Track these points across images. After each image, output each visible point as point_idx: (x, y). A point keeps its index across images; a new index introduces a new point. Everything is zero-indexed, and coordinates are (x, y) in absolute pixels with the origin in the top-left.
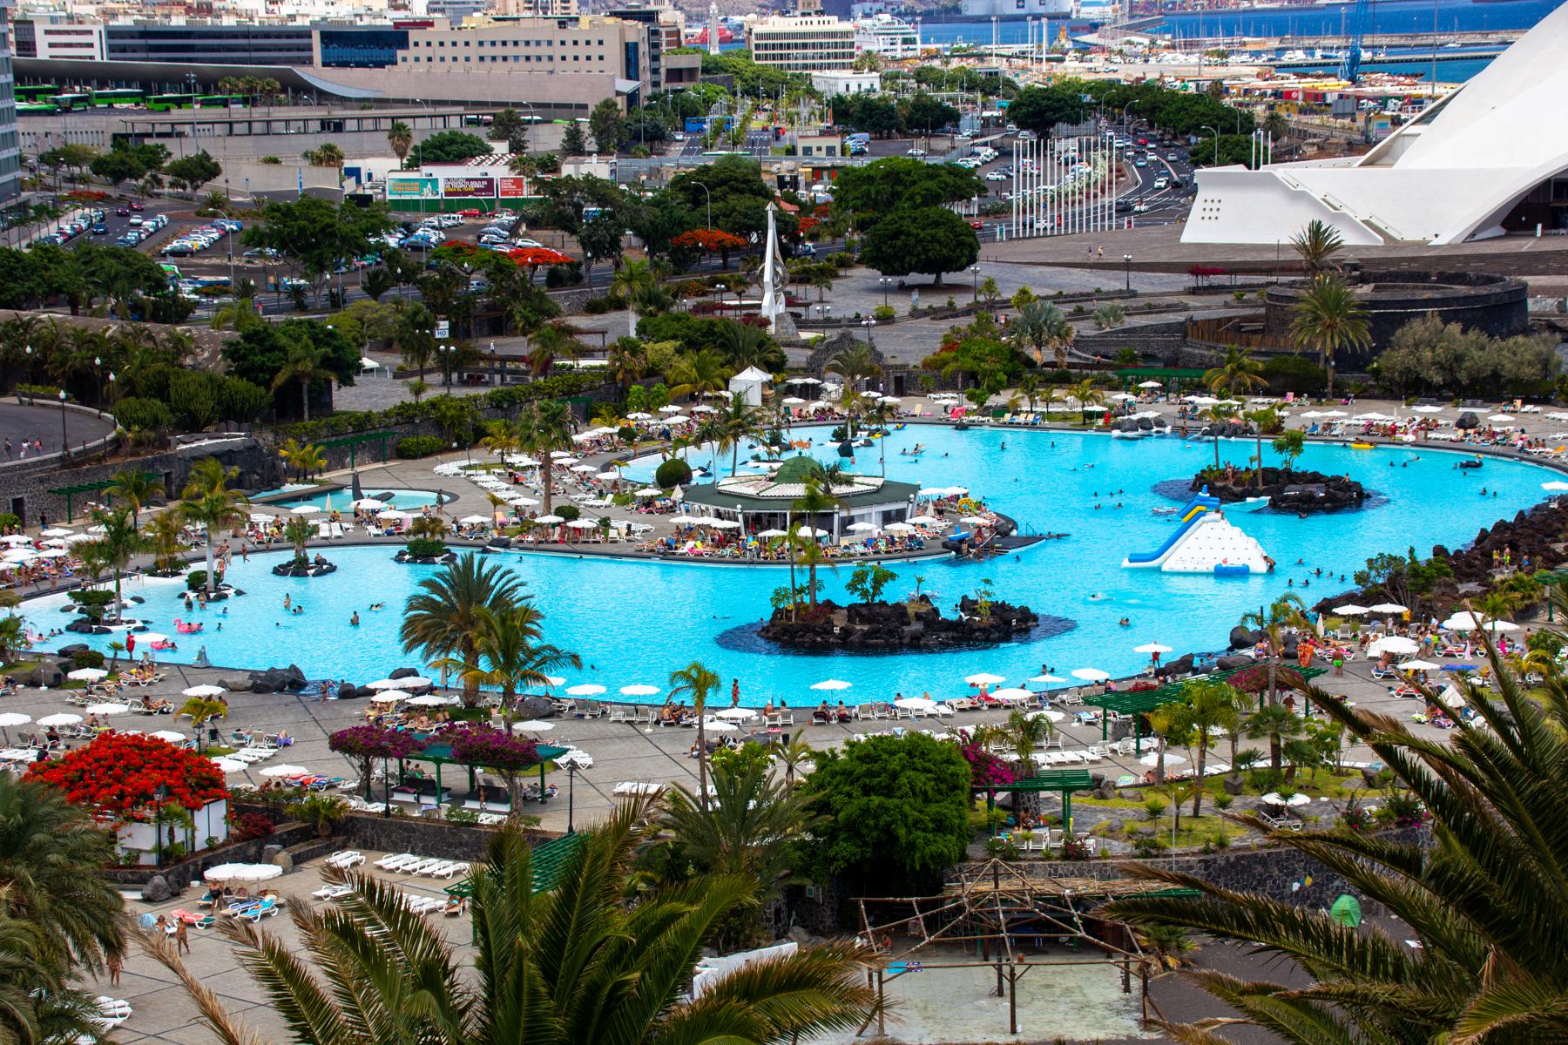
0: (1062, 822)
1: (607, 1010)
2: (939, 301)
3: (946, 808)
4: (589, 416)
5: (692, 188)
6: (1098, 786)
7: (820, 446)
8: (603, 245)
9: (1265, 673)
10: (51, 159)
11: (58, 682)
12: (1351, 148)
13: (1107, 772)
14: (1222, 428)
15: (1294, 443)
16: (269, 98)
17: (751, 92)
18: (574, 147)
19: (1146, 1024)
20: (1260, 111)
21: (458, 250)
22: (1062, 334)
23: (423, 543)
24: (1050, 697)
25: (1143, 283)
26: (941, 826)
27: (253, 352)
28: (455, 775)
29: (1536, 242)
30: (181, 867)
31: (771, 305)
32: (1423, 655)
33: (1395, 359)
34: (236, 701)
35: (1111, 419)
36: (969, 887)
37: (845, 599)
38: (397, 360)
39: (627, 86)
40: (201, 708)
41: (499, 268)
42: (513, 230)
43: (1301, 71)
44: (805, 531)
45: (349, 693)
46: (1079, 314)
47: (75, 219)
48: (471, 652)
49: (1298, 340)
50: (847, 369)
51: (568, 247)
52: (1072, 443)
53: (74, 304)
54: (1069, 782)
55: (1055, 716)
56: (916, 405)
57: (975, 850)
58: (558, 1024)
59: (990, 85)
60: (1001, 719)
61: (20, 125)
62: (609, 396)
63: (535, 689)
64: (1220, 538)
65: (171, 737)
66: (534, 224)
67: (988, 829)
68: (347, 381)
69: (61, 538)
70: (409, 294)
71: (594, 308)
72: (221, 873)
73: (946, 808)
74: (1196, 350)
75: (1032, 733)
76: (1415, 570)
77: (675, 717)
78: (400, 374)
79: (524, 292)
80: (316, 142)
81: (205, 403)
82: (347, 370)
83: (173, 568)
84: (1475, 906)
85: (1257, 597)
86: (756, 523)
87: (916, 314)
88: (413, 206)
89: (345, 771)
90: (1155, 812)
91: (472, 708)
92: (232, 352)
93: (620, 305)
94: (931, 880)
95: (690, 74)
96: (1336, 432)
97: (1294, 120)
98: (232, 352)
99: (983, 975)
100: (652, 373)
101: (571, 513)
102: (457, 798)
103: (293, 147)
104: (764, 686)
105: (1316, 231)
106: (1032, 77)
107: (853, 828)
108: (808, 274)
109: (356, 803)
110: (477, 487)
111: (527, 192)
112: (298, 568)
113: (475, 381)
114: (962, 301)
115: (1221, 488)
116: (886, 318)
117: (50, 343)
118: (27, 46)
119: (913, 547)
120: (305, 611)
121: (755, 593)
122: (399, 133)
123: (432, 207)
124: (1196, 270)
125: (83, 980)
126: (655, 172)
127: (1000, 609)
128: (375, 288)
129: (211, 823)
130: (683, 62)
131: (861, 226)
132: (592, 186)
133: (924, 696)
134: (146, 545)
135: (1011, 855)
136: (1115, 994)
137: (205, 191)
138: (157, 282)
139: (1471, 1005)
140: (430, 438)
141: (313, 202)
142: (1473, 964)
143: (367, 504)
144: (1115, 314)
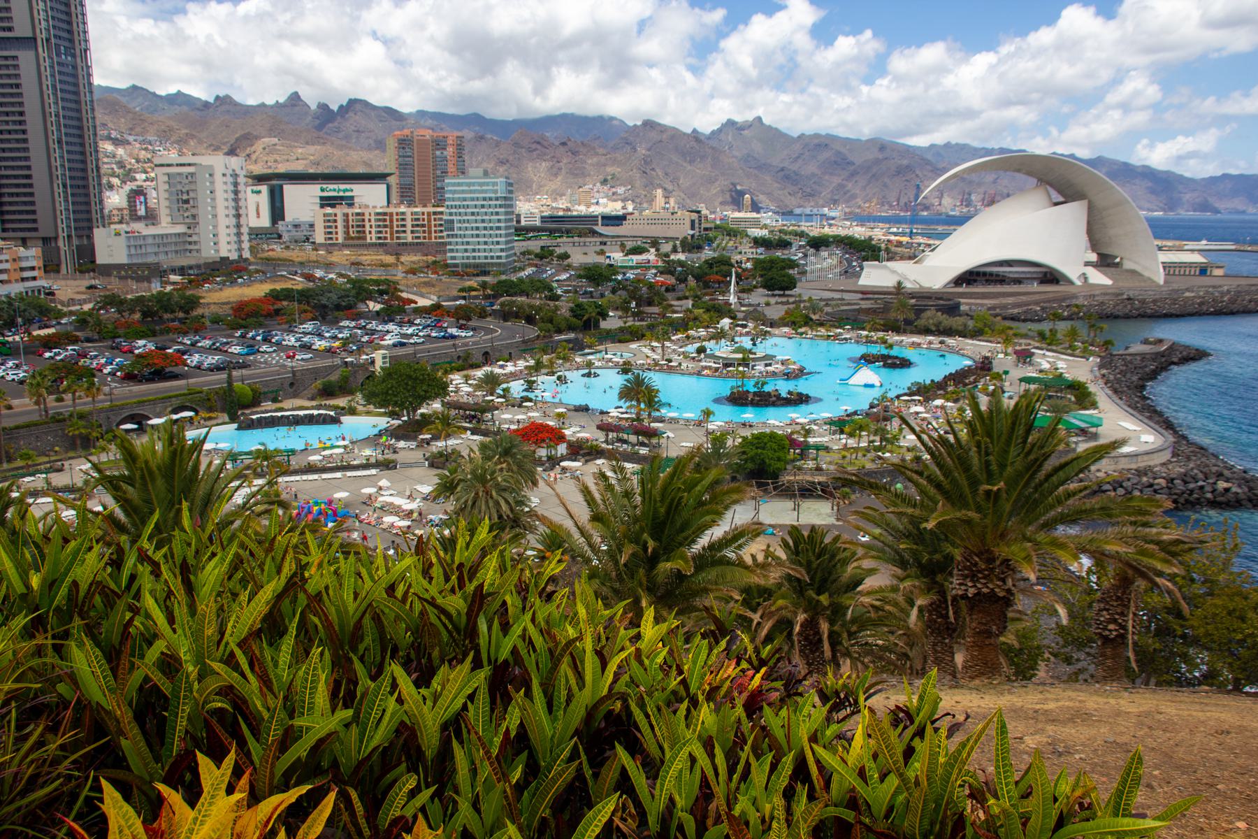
0: (816, 459)
1: (677, 506)
2: (784, 299)
3: (781, 454)
4: (677, 330)
5: (710, 264)
6: (827, 449)
7: (746, 342)
8: (682, 280)
9: (879, 416)
10: (523, 254)
11: (520, 406)
12: (910, 258)
13: (830, 445)
14: (869, 341)
15: (891, 347)
16: (585, 235)
17: (729, 235)
18: (675, 250)
19: (838, 520)
20: (883, 246)
21: (639, 281)
22: (822, 311)
23: (625, 369)
24: (814, 422)
25: (847, 296)
26: (779, 459)
27: (577, 311)
28: (633, 438)
29: (963, 289)
30: (553, 461)
31: (732, 299)
32: (927, 412)
33: (921, 322)
34: (569, 414)
35: (836, 337)
36: (786, 478)
37: (752, 390)
38: (620, 313)
39: (691, 232)
40: (560, 415)
41: (651, 286)
42: (656, 275)
43: (895, 234)
44: (741, 369)
45: (602, 413)
46: (827, 305)
47: (529, 271)
48: (638, 401)
49: (893, 315)
50: (755, 319)
51: (671, 280)
52: (823, 344)
53: (527, 296)
54: (818, 448)
55: (815, 428)
56: (776, 331)
57: (789, 467)
58: (662, 510)
59: (802, 235)
60: (798, 428)
61: (515, 244)
62: (682, 326)
63: (657, 414)
64: (868, 375)
65: (551, 423)
66: (662, 273)
67: (793, 461)
68: (604, 319)
69: (521, 364)
70: (623, 293)
71: (679, 299)
72: (564, 464)
73: (781, 454)
74: (862, 317)
75: (808, 432)
76: (925, 387)
77: (699, 424)
78: (620, 317)
79: (658, 293)
80: (598, 248)
81: (563, 325)
82: (604, 316)
83: (553, 374)
84: (938, 486)
85: (876, 393)
86: (726, 365)
87: (777, 303)
88: (626, 267)
89: (601, 436)
90: (844, 457)
91: (638, 419)
92: (572, 310)
93: (687, 298)
94: (775, 476)
95: (710, 229)
96: (903, 344)
97: (893, 249)
98: (572, 310)
99: (789, 504)
100: (696, 319)
101: (670, 361)
102: (634, 445)
103: (592, 249)
104: (723, 417)
105: (899, 283)
106: (815, 232)
107: (752, 459)
108: (744, 291)
109: (604, 445)
110: (641, 352)
111: (660, 264)
112: (589, 375)
113: (642, 320)
114: (791, 300)
115: (868, 359)
116: (768, 304)
117: (520, 307)
118: (518, 221)
119: (774, 374)
120: (589, 388)
121: (725, 387)
122: (623, 246)
123: (632, 268)
124: (863, 293)
125: (526, 492)
126: (699, 258)
127: (800, 395)
128: (614, 291)
129: (562, 449)
130: (708, 226)
131: (761, 276)
132: (681, 263)
133: (776, 420)
134: (545, 367)
135: (800, 469)
136: (829, 511)
137: (566, 263)
138: (551, 289)
139: (934, 515)
140: (628, 337)
141: (597, 266)
142: (936, 503)
143: (609, 356)
144: (838, 305)
